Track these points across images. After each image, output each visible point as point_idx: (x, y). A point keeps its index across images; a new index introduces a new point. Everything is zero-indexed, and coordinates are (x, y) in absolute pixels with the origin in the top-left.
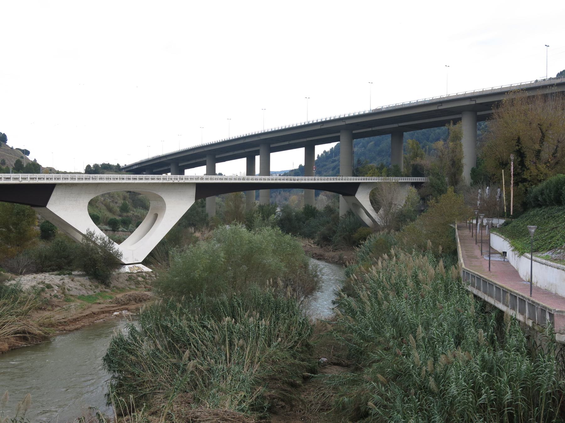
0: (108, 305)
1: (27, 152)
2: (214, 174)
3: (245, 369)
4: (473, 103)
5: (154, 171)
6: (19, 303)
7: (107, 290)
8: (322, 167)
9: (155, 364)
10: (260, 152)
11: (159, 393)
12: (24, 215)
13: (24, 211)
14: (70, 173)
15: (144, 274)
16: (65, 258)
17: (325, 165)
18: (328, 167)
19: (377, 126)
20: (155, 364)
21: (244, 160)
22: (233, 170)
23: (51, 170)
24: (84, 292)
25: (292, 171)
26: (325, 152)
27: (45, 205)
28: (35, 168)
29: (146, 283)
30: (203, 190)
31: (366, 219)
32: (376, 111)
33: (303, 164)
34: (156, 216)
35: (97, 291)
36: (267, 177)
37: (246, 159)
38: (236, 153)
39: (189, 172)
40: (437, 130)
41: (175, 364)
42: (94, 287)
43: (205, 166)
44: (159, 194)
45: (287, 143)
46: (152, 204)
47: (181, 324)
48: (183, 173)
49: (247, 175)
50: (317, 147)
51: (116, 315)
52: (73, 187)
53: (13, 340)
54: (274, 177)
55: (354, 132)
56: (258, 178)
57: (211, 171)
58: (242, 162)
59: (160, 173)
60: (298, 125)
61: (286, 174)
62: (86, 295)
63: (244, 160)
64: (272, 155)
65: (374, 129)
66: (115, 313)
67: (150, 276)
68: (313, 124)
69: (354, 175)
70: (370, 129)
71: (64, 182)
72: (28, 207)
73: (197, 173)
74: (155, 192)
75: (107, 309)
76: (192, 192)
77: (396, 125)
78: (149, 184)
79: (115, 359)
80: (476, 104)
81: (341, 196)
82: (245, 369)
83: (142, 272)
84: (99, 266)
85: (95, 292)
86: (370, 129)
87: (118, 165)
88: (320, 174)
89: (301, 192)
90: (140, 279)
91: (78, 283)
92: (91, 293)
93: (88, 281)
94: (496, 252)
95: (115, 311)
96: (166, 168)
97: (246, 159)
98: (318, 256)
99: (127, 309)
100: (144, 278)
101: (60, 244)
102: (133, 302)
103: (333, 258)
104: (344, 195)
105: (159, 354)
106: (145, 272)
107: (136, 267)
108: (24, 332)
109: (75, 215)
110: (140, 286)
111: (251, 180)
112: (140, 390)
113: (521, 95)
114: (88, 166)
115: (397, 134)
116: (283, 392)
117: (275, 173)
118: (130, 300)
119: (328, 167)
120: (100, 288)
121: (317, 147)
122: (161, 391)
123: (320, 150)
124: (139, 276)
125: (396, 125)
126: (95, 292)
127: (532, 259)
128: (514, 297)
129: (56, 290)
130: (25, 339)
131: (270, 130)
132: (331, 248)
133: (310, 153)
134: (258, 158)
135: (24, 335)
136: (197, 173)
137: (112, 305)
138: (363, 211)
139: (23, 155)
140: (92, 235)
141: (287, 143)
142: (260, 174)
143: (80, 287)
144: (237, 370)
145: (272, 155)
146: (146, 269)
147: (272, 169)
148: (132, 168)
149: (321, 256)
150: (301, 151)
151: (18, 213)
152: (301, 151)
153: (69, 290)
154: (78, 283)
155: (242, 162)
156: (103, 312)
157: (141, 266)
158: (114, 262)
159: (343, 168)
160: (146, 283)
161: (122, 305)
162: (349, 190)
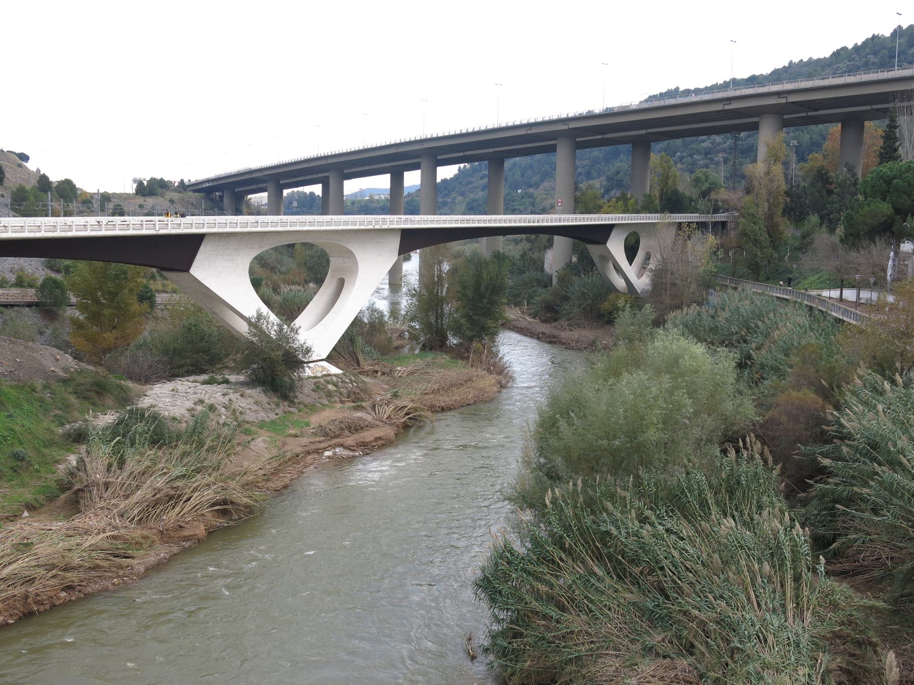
0: (313, 440)
1: (24, 157)
3: (791, 620)
4: (783, 101)
6: (208, 450)
7: (292, 409)
8: (467, 185)
9: (591, 601)
11: (607, 654)
12: (125, 278)
13: (125, 272)
15: (334, 378)
16: (204, 352)
17: (470, 183)
18: (475, 185)
20: (591, 601)
24: (262, 415)
27: (187, 269)
29: (341, 394)
31: (619, 283)
32: (621, 110)
34: (341, 284)
35: (279, 411)
41: (634, 603)
42: (274, 406)
44: (349, 247)
46: (334, 263)
51: (329, 457)
53: (209, 517)
55: (578, 139)
62: (267, 419)
65: (605, 136)
66: (327, 453)
67: (343, 382)
70: (600, 137)
71: (221, 230)
72: (132, 266)
74: (342, 244)
75: (313, 447)
76: (395, 243)
77: (643, 132)
78: (343, 231)
79: (505, 588)
80: (787, 103)
82: (791, 620)
83: (329, 375)
84: (273, 368)
85: (277, 414)
86: (600, 137)
90: (330, 387)
91: (251, 401)
92: (273, 416)
93: (263, 395)
95: (325, 449)
98: (549, 336)
99: (342, 445)
100: (336, 386)
101: (193, 329)
102: (347, 432)
103: (578, 341)
105: (597, 584)
106: (335, 375)
108: (225, 502)
110: (333, 400)
112: (564, 647)
114: (140, 183)
116: (852, 659)
118: (342, 429)
119: (475, 185)
120: (282, 407)
122: (611, 652)
124: (328, 382)
125: (643, 132)
126: (277, 414)
129: (224, 416)
130: (224, 513)
132: (564, 322)
135: (225, 507)
137: (317, 439)
139: (20, 162)
140: (260, 316)
143: (255, 407)
144: (776, 624)
146: (334, 370)
148: (200, 187)
149: (554, 337)
151: (117, 276)
153: (241, 413)
154: (251, 401)
156: (309, 453)
157: (325, 364)
158: (294, 359)
160: (341, 394)
161: (332, 438)
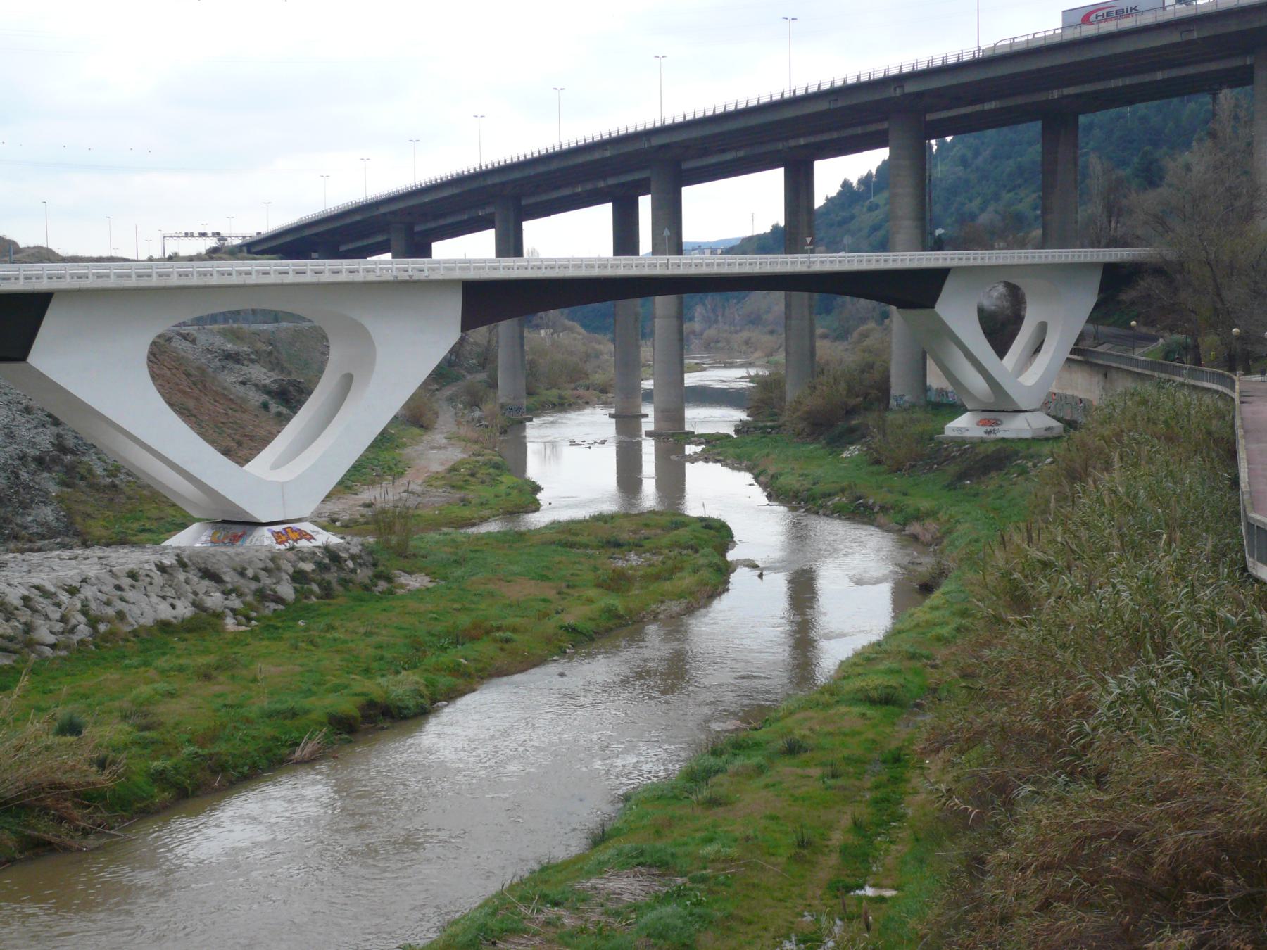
5: (343, 248)
10: (497, 220)
19: (726, 162)
21: (604, 213)
22: (572, 239)
23: (43, 255)
25: (750, 239)
30: (485, 300)
33: (782, 224)
34: (347, 382)
36: (674, 259)
37: (610, 205)
38: (442, 222)
39: (447, 251)
40: (1194, 106)
43: (493, 231)
45: (566, 192)
47: (1030, 905)
48: (426, 252)
52: (115, 295)
56: (647, 258)
57: (510, 245)
59: (362, 253)
60: (762, 101)
63: (604, 213)
68: (808, 98)
73: (471, 251)
76: (453, 307)
81: (894, 308)
89: (776, 300)
96: (379, 238)
97: (610, 205)
107: (293, 530)
109: (104, 381)
111: (627, 267)
115: (1059, 123)
117: (700, 248)
123: (833, 175)
131: (679, 119)
133: (799, 187)
134: (645, 204)
136: (471, 251)
138: (959, 354)
142: (655, 251)
145: (528, 226)
150: (774, 179)
152: (774, 179)
162: (917, 290)
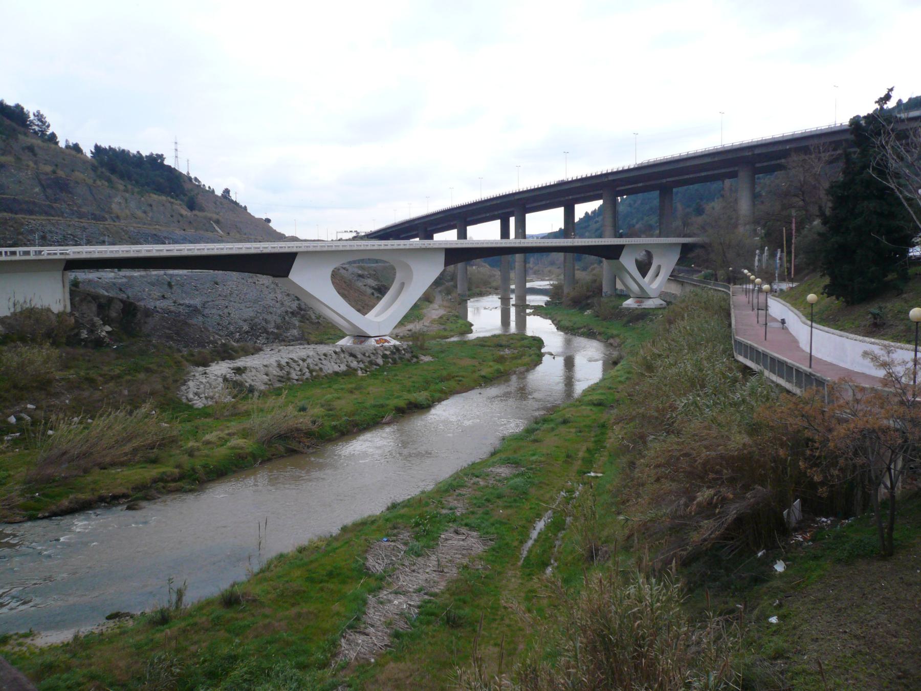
2: (524, 236)
14: (305, 241)
21: (497, 223)
22: (485, 233)
23: (294, 239)
26: (587, 214)
28: (281, 237)
30: (453, 255)
36: (523, 240)
39: (438, 237)
45: (544, 203)
48: (432, 238)
49: (502, 238)
50: (577, 206)
52: (319, 253)
54: (530, 240)
57: (462, 235)
58: (496, 225)
61: (537, 237)
63: (497, 223)
64: (528, 216)
69: (615, 237)
73: (448, 237)
76: (441, 258)
87: (472, 325)
88: (582, 236)
94: (775, 320)
104: (607, 258)
109: (316, 285)
111: (505, 243)
113: (823, 140)
115: (666, 191)
117: (532, 236)
121: (577, 206)
123: (582, 210)
127: (812, 327)
128: (790, 368)
134: (512, 220)
136: (448, 237)
141: (544, 203)
142: (516, 237)
145: (528, 216)
147: (529, 231)
150: (560, 212)
152: (560, 212)
155: (496, 225)
159: (609, 229)
162: (613, 253)
